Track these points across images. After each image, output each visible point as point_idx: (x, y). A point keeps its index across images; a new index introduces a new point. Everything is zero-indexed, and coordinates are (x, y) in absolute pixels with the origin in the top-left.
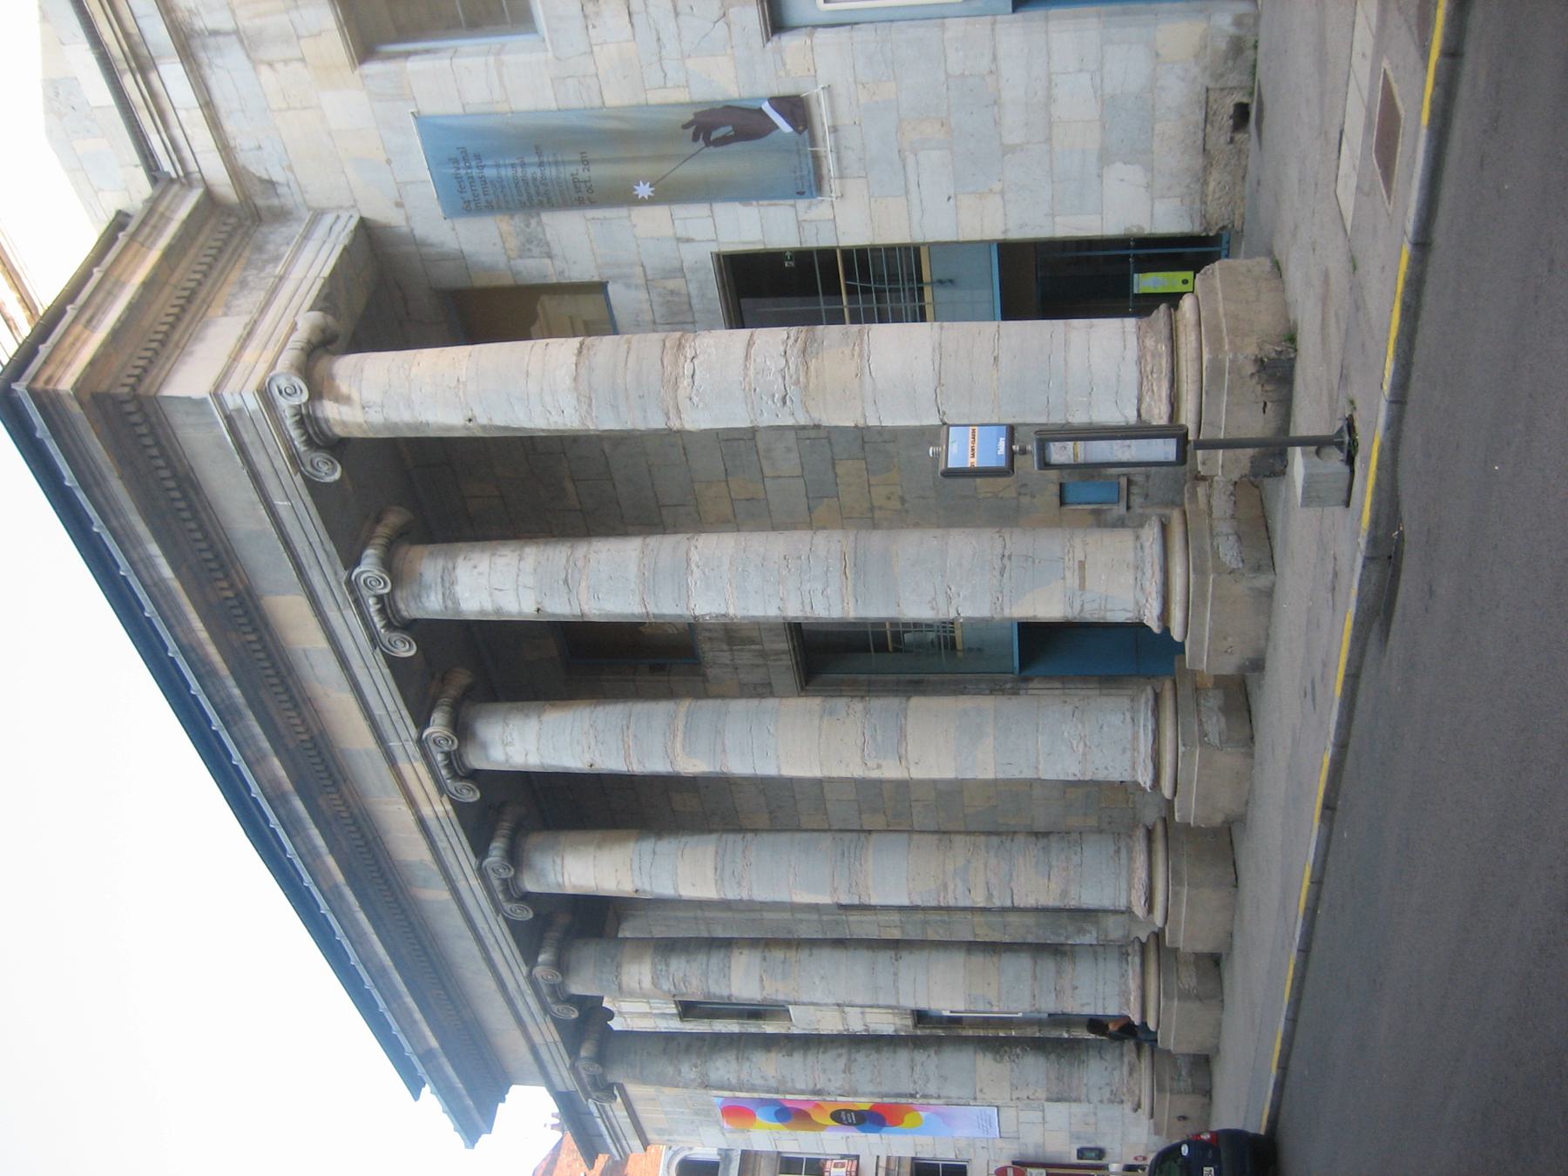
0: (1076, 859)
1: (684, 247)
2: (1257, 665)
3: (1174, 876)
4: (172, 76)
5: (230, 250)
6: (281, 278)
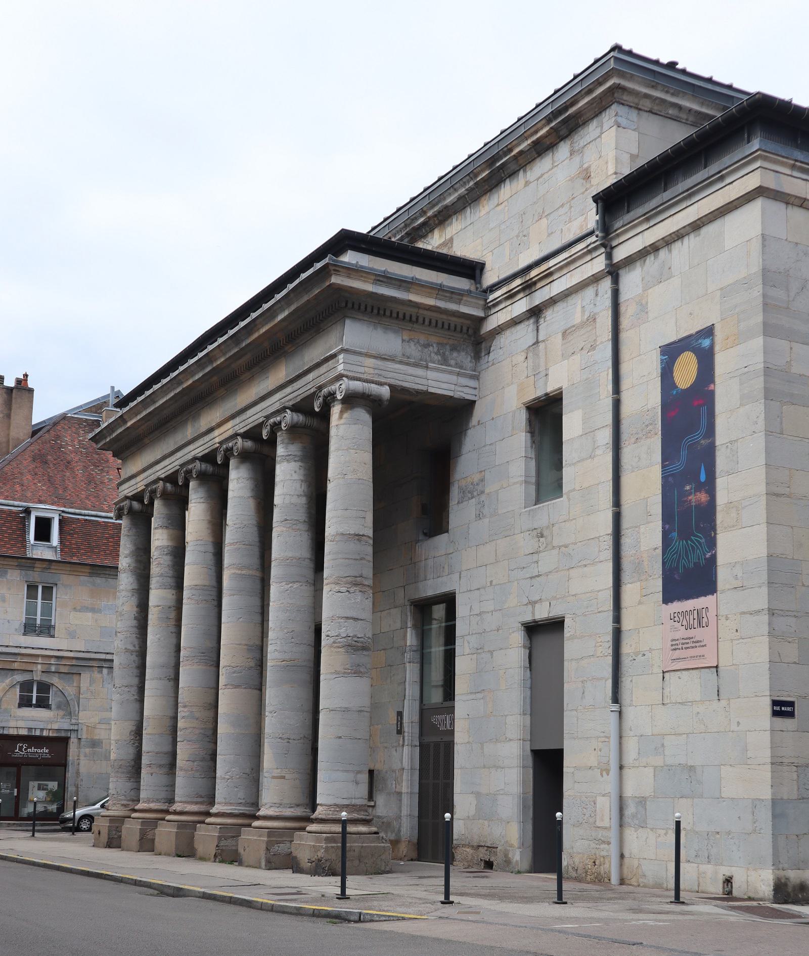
2: (241, 864)
4: (521, 306)
6: (427, 367)
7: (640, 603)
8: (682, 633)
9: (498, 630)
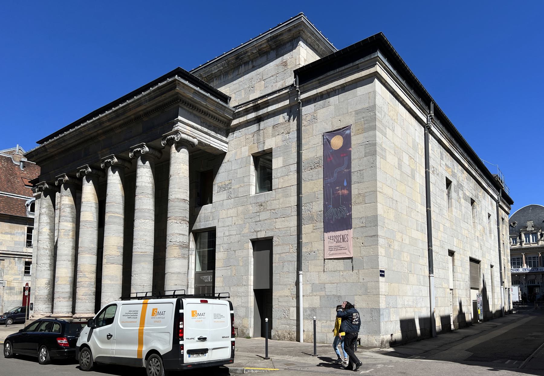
1: (217, 220)
7: (312, 232)
8: (334, 244)
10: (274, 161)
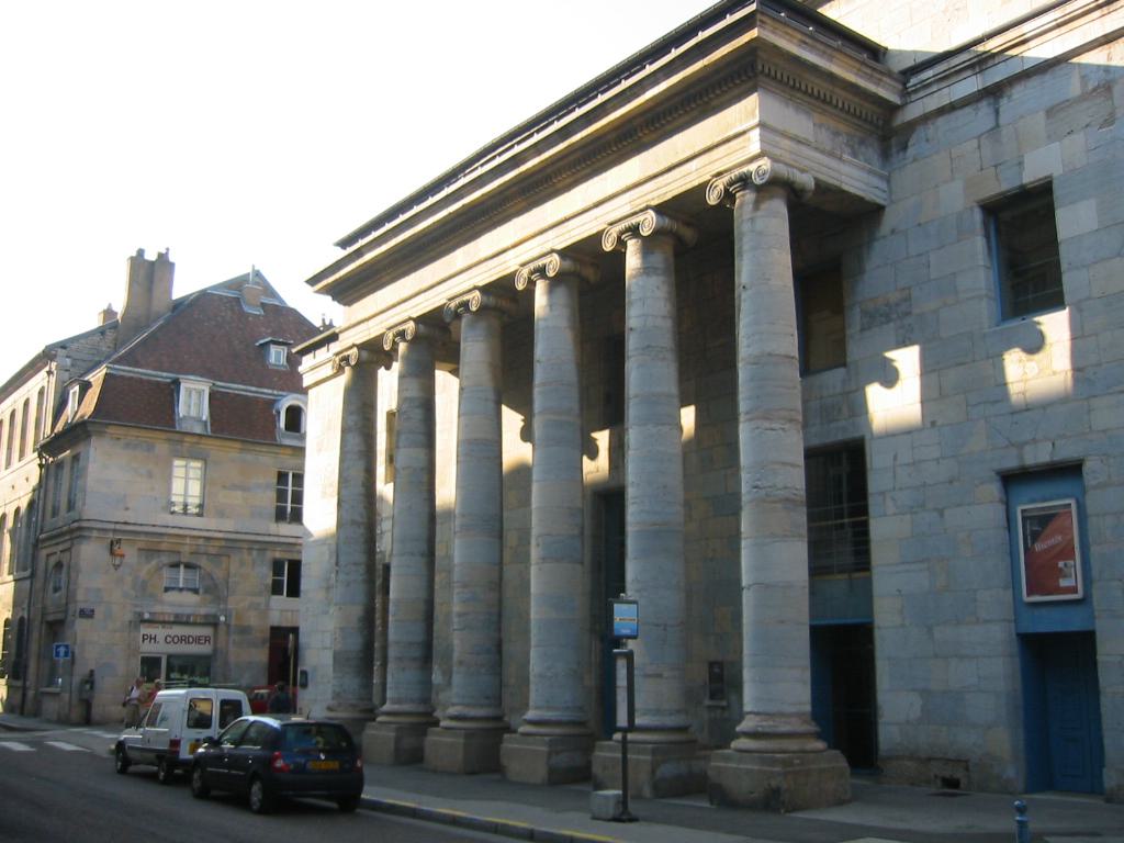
0: (483, 671)
3: (469, 734)
5: (860, 123)
6: (840, 159)
9: (951, 482)
10: (1062, 216)
